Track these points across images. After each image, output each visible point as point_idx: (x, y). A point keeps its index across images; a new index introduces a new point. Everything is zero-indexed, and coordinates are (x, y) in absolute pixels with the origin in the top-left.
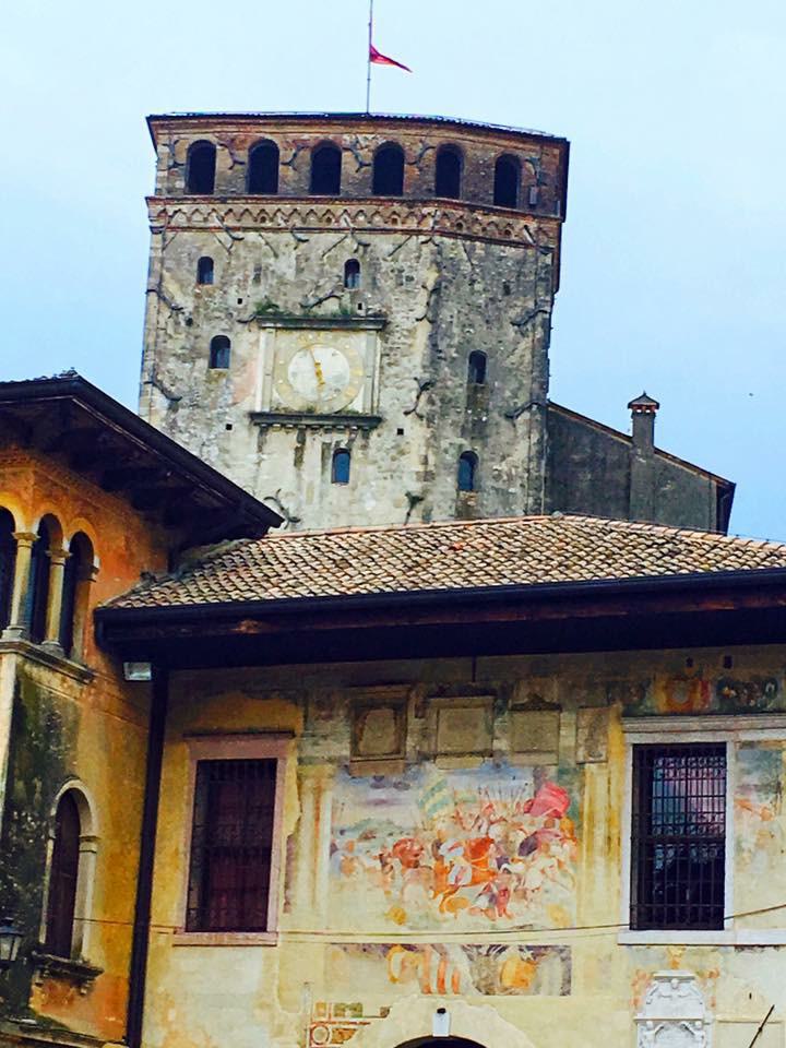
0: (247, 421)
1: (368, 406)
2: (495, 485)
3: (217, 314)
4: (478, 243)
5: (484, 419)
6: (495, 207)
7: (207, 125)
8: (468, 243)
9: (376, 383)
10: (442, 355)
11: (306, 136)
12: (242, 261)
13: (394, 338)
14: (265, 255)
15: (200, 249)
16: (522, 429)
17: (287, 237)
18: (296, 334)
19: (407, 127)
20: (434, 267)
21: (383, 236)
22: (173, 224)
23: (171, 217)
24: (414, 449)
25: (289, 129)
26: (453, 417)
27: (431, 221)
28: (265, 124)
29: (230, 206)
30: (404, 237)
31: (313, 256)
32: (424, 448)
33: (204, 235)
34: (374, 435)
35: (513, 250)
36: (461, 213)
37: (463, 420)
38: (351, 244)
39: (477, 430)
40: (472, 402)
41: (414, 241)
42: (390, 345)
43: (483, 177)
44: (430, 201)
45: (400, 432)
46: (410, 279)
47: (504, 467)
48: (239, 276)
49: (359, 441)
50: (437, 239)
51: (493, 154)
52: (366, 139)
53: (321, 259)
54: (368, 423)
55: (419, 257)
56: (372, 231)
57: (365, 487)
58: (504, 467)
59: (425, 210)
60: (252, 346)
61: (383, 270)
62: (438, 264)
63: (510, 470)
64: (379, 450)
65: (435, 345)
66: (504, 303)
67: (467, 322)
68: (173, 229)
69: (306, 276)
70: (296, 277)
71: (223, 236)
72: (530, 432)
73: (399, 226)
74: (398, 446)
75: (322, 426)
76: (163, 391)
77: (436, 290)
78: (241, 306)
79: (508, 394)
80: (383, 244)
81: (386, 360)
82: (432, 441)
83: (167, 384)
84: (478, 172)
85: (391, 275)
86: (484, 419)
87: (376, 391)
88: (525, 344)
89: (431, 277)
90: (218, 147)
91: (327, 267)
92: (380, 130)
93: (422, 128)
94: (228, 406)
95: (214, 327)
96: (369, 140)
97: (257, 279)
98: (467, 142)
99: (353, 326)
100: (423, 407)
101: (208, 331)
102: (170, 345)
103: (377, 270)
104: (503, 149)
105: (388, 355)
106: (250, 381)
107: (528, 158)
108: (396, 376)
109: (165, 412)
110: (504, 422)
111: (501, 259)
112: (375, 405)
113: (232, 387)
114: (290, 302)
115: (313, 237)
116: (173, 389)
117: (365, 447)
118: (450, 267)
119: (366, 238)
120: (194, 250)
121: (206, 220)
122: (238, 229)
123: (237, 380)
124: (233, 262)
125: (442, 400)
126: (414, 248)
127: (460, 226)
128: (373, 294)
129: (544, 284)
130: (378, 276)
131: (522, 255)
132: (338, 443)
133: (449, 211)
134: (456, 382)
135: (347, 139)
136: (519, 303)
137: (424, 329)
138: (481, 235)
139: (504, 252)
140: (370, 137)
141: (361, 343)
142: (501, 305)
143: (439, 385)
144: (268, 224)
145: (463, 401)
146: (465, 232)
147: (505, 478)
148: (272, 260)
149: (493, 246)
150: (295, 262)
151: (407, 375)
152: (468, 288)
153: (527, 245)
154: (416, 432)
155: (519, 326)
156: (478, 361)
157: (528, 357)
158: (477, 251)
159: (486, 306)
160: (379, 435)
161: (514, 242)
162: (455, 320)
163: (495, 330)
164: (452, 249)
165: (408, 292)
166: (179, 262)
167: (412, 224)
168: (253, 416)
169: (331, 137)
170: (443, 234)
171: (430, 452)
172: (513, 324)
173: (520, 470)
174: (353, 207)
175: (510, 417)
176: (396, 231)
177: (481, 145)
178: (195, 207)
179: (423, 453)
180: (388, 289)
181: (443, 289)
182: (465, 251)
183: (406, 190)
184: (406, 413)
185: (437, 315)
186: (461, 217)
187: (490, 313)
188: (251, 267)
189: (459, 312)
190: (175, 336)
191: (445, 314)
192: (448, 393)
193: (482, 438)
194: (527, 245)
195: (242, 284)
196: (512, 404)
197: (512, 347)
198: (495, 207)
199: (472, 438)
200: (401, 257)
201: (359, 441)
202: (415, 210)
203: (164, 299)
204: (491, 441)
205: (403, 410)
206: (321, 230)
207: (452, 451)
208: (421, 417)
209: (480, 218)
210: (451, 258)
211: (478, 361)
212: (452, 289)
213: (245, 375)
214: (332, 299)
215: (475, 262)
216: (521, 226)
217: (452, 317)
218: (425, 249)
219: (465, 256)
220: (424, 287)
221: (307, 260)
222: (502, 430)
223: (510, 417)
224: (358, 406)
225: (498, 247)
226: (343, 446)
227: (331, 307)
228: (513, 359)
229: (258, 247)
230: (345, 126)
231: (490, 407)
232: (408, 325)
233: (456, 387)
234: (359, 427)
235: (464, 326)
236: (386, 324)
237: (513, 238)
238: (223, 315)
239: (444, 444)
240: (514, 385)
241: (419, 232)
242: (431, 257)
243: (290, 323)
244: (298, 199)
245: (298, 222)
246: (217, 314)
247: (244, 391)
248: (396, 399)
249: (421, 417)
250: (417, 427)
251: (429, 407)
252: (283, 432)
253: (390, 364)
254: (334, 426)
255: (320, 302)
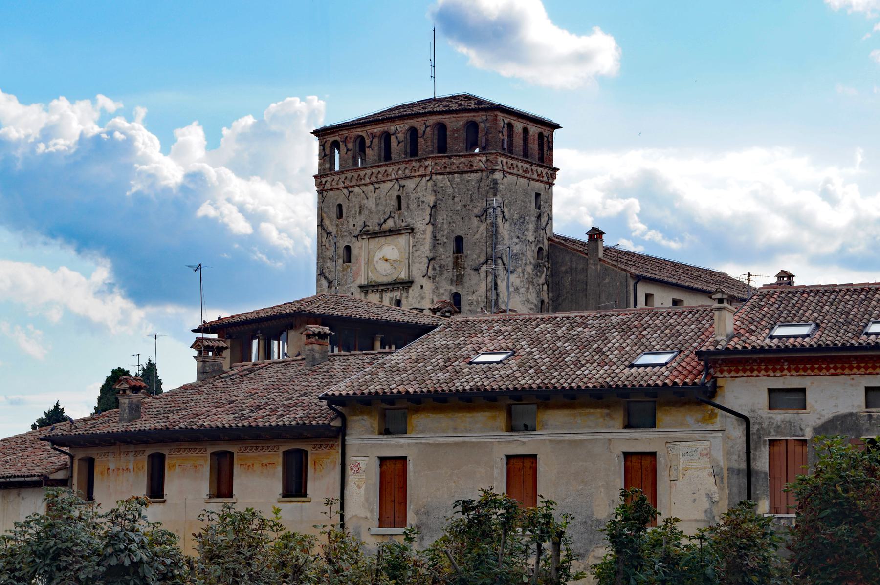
0: (359, 290)
1: (407, 275)
2: (470, 308)
3: (345, 234)
4: (456, 175)
5: (463, 273)
6: (439, 155)
7: (334, 133)
8: (451, 176)
9: (410, 262)
10: (439, 242)
11: (376, 131)
12: (354, 204)
13: (417, 236)
14: (363, 199)
15: (336, 200)
16: (483, 275)
17: (371, 187)
18: (377, 240)
19: (417, 117)
20: (433, 194)
21: (410, 180)
22: (325, 188)
23: (325, 184)
24: (427, 295)
25: (368, 128)
26: (446, 275)
27: (430, 168)
28: (357, 128)
29: (346, 175)
30: (420, 179)
31: (382, 196)
32: (432, 295)
33: (338, 192)
34: (411, 289)
35: (475, 174)
36: (444, 161)
37: (451, 277)
38: (397, 186)
39: (459, 280)
40: (456, 264)
41: (424, 180)
42: (416, 240)
43: (457, 137)
44: (428, 158)
45: (422, 287)
46: (423, 202)
47: (474, 298)
48: (353, 212)
49: (405, 295)
50: (434, 177)
51: (461, 123)
52: (400, 127)
53: (386, 197)
54: (407, 284)
55: (426, 189)
56: (406, 178)
57: (447, 298)
58: (474, 298)
59: (427, 163)
60: (360, 248)
61: (411, 199)
62: (435, 192)
63: (478, 299)
64: (413, 298)
65: (435, 237)
66: (471, 206)
67: (451, 221)
68: (326, 190)
69: (380, 208)
70: (376, 208)
71: (345, 191)
72: (487, 276)
73: (417, 174)
74: (421, 295)
75: (388, 289)
76: (326, 278)
77: (434, 206)
78: (354, 228)
79: (475, 256)
80: (410, 184)
81: (414, 248)
82: (435, 290)
83: (327, 275)
84: (454, 134)
85: (415, 201)
86: (463, 273)
87: (411, 266)
88: (483, 227)
89: (431, 199)
90: (341, 143)
91: (388, 201)
92: (406, 121)
93: (423, 117)
94: (352, 283)
95: (344, 241)
96: (402, 127)
97: (360, 212)
98: (446, 119)
99: (399, 232)
100: (431, 272)
101: (342, 244)
102: (327, 253)
103: (409, 199)
104: (467, 118)
105: (415, 245)
106: (359, 268)
107: (480, 120)
108: (419, 256)
109: (327, 289)
110: (472, 272)
111: (468, 181)
112: (410, 274)
113: (352, 272)
114: (373, 226)
115: (382, 185)
116: (330, 277)
117: (407, 297)
118: (441, 192)
119: (402, 182)
120: (334, 201)
121: (338, 184)
122: (350, 187)
123: (354, 268)
124: (350, 205)
125: (440, 267)
126: (424, 184)
127: (445, 167)
128: (408, 212)
129: (492, 190)
130: (410, 203)
131: (480, 177)
132: (396, 296)
133: (437, 161)
134: (447, 254)
135: (392, 129)
136: (479, 204)
137: (430, 228)
138: (457, 170)
139: (470, 177)
140: (402, 126)
141: (402, 240)
142: (470, 207)
143: (438, 258)
144: (363, 182)
145: (451, 265)
146: (448, 170)
147: (475, 303)
148: (366, 201)
149: (464, 175)
150: (374, 200)
151: (423, 256)
152: (451, 202)
153: (482, 171)
154: (428, 285)
155: (479, 217)
156: (459, 241)
157: (485, 234)
158: (456, 180)
159: (462, 210)
160: (413, 290)
161: (474, 171)
162: (445, 221)
163: (466, 223)
164: (442, 181)
165: (422, 209)
166: (328, 207)
167: (422, 171)
168: (360, 287)
169: (386, 129)
170: (436, 174)
171: (435, 296)
172: (476, 217)
173: (483, 298)
174: (396, 167)
175: (476, 269)
176: (415, 177)
177: (455, 119)
178: (333, 178)
179: (431, 298)
180: (414, 209)
181: (438, 205)
182: (449, 181)
183: (420, 153)
184: (424, 277)
185: (435, 220)
186: (445, 163)
187: (464, 213)
188: (357, 206)
189: (447, 216)
190: (329, 248)
191: (440, 219)
192: (443, 262)
193: (462, 284)
194: (482, 171)
195: (354, 217)
196: (477, 262)
197: (476, 230)
198: (439, 155)
199: (457, 284)
200: (419, 190)
201: (405, 295)
202: (422, 163)
203: (324, 229)
204: (466, 285)
205: (422, 275)
206: (384, 181)
207: (447, 294)
208: (430, 278)
209: (455, 161)
210: (442, 187)
211: (459, 241)
212: (443, 204)
213: (358, 265)
214: (390, 219)
215: (454, 186)
216: (477, 161)
217: (443, 219)
218: (429, 184)
219: (449, 183)
220: (429, 205)
221: (380, 199)
222: (472, 277)
223: (476, 269)
224: (403, 276)
225: (466, 175)
226: (398, 298)
227: (390, 224)
228: (477, 236)
229: (360, 195)
230: (391, 122)
231: (466, 266)
232: (423, 227)
233: (447, 258)
234: (403, 287)
235: (450, 223)
236: (412, 229)
237: (475, 168)
238: (348, 234)
239: (442, 291)
240: (477, 251)
241: (425, 175)
242: (431, 188)
243: (374, 235)
244: (374, 167)
245: (374, 179)
246: (345, 234)
247: (357, 274)
248: (418, 270)
249: (430, 278)
250: (428, 283)
251: (433, 272)
252: (374, 294)
253: (416, 251)
254: (393, 288)
255: (385, 221)
